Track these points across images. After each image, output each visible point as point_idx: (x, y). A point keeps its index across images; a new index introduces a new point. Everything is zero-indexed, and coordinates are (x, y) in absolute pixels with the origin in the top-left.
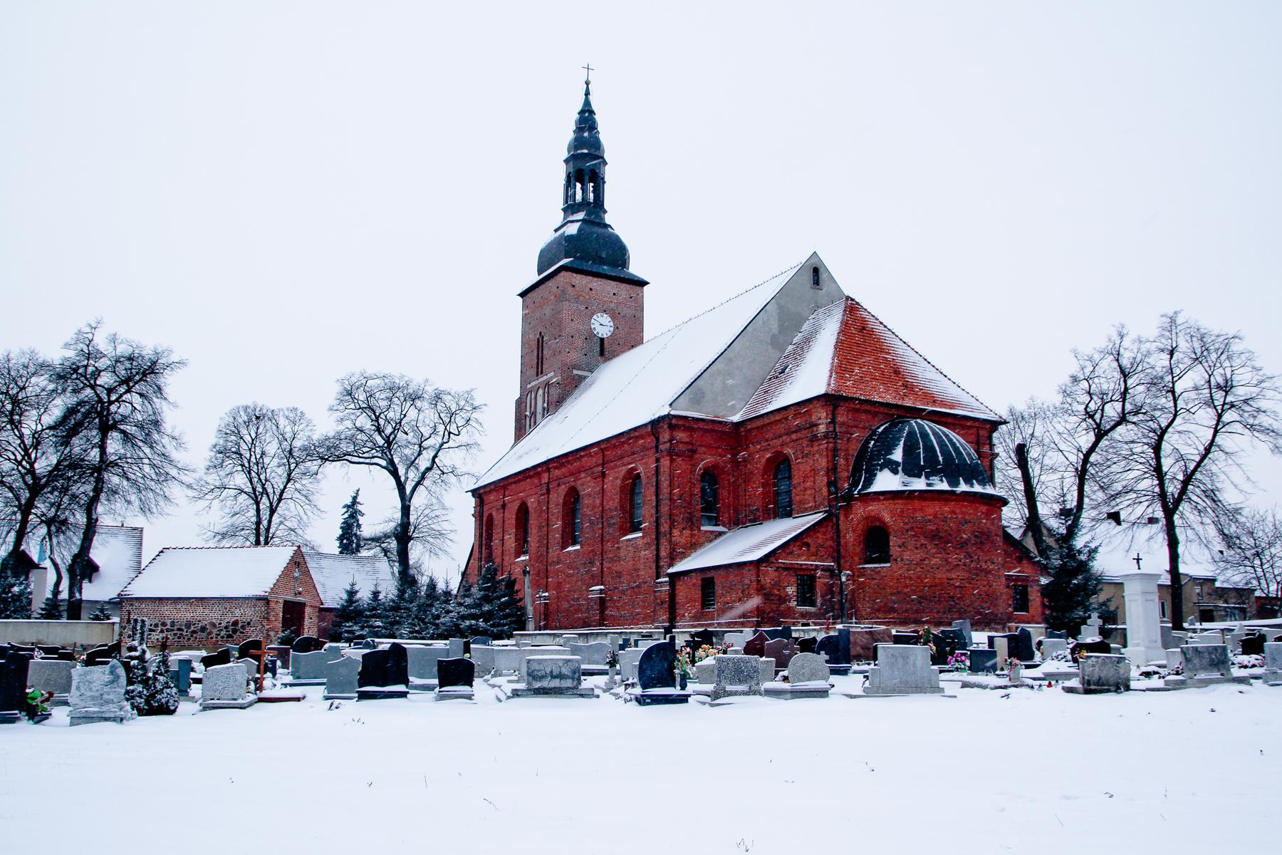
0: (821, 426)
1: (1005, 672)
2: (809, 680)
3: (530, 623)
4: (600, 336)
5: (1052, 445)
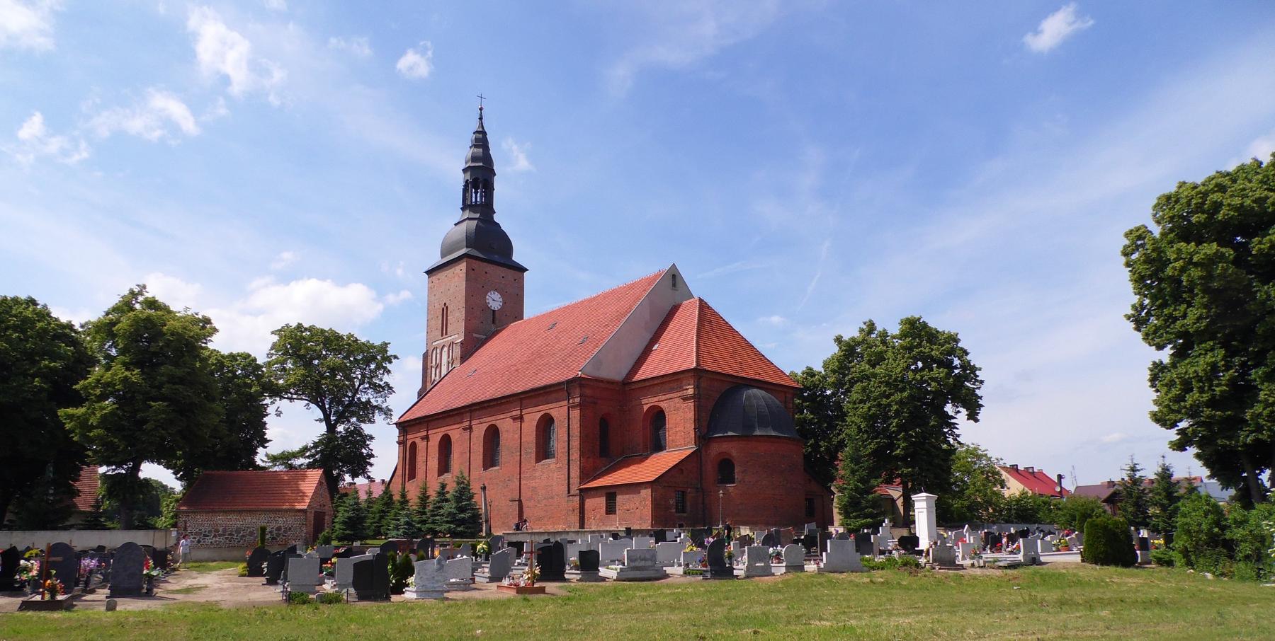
4: (493, 308)
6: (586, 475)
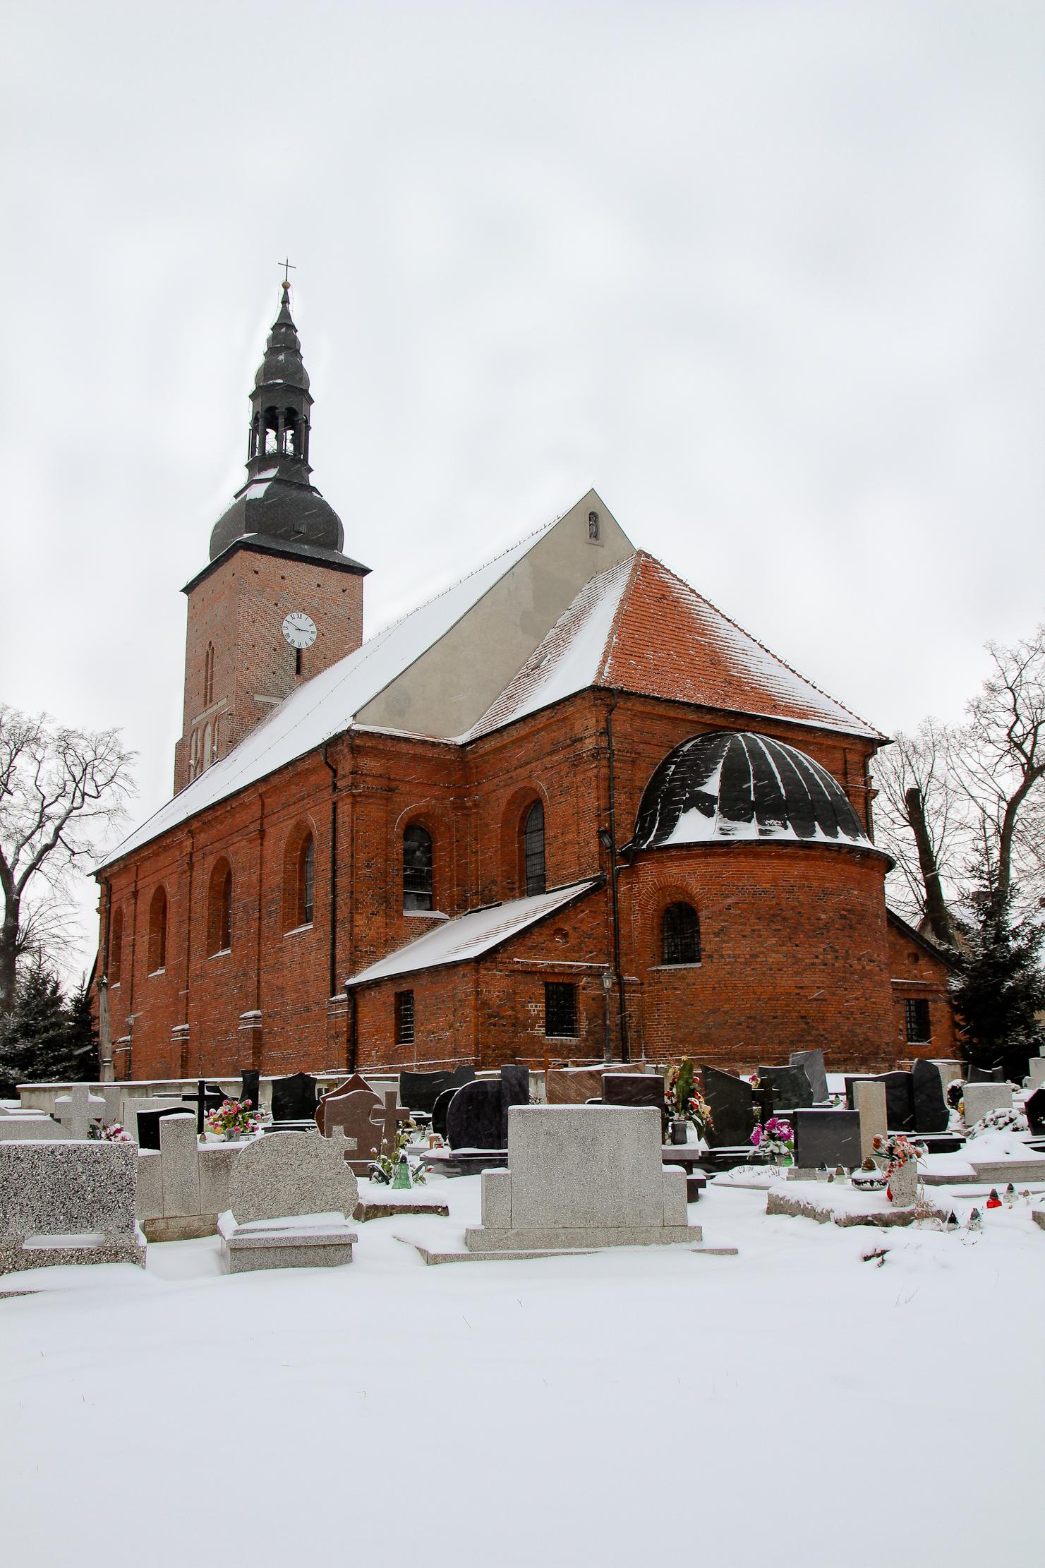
0: (587, 741)
1: (878, 1174)
2: (292, 1211)
3: (107, 1070)
4: (296, 645)
5: (961, 790)
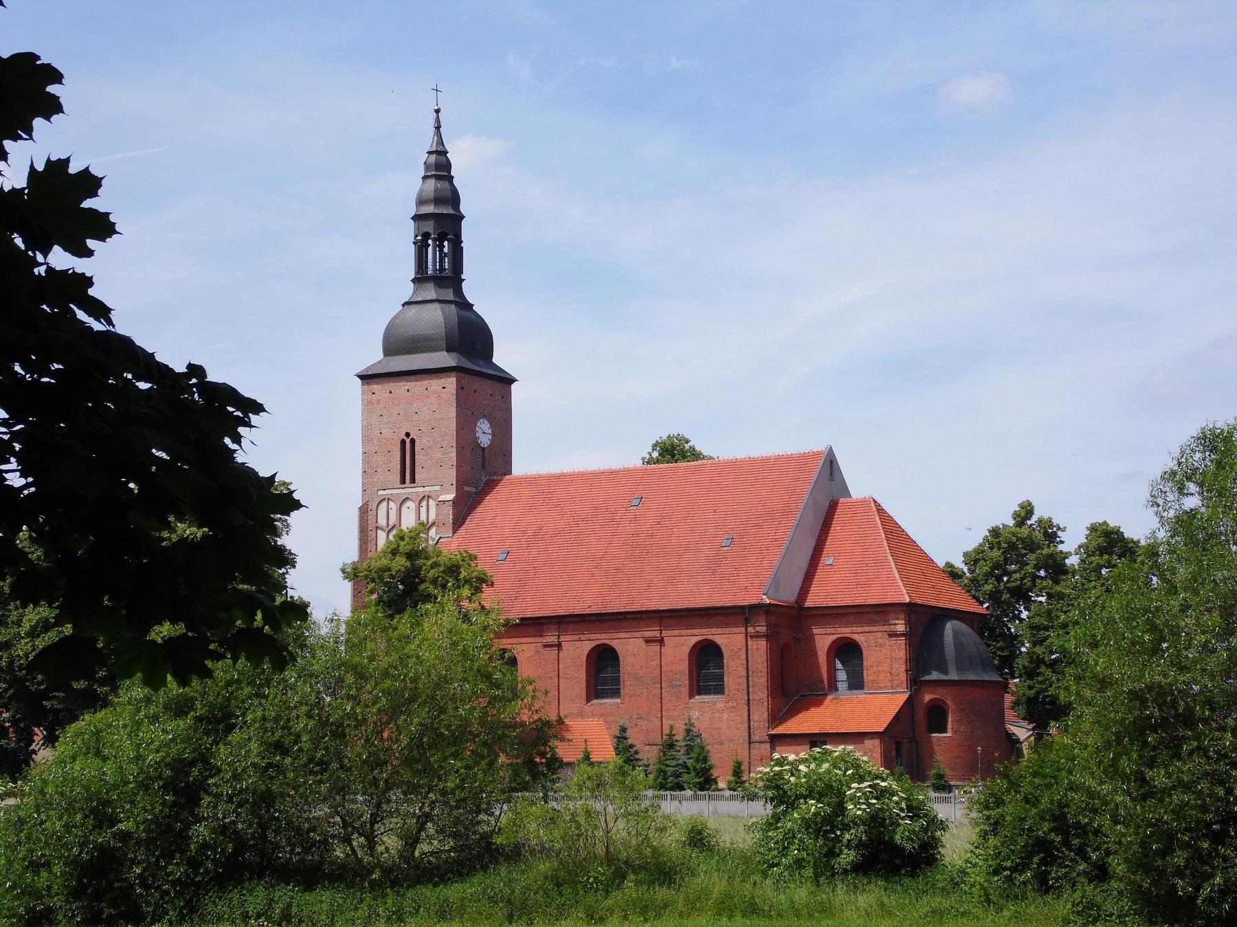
6: (777, 717)
